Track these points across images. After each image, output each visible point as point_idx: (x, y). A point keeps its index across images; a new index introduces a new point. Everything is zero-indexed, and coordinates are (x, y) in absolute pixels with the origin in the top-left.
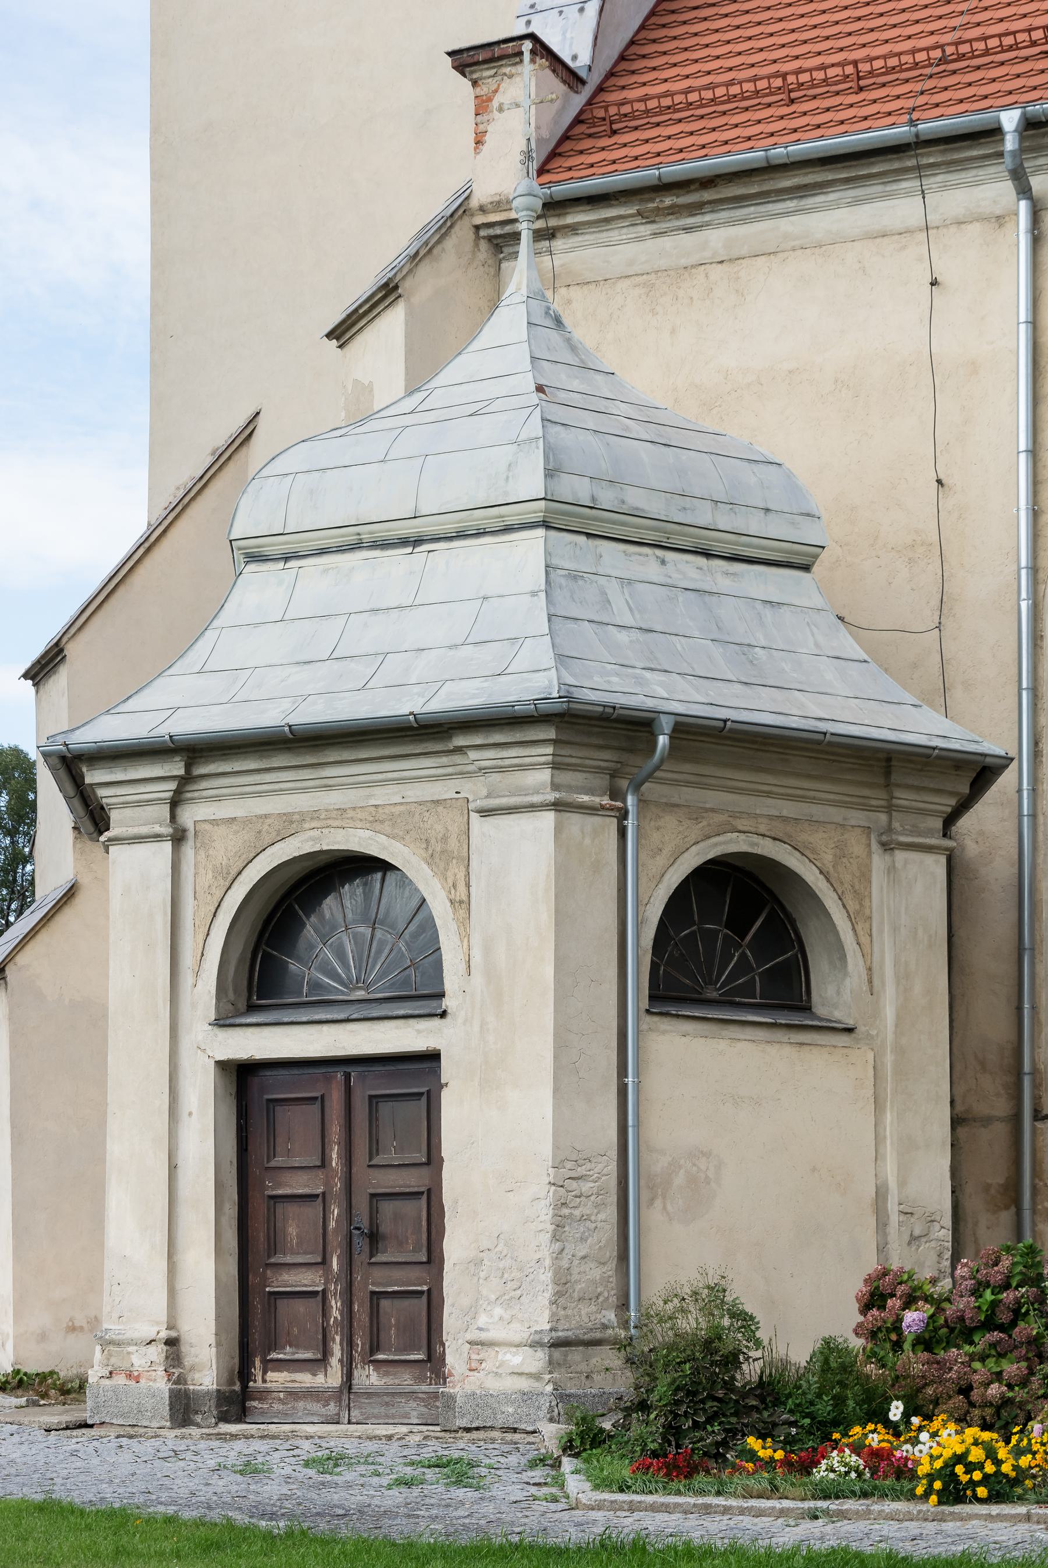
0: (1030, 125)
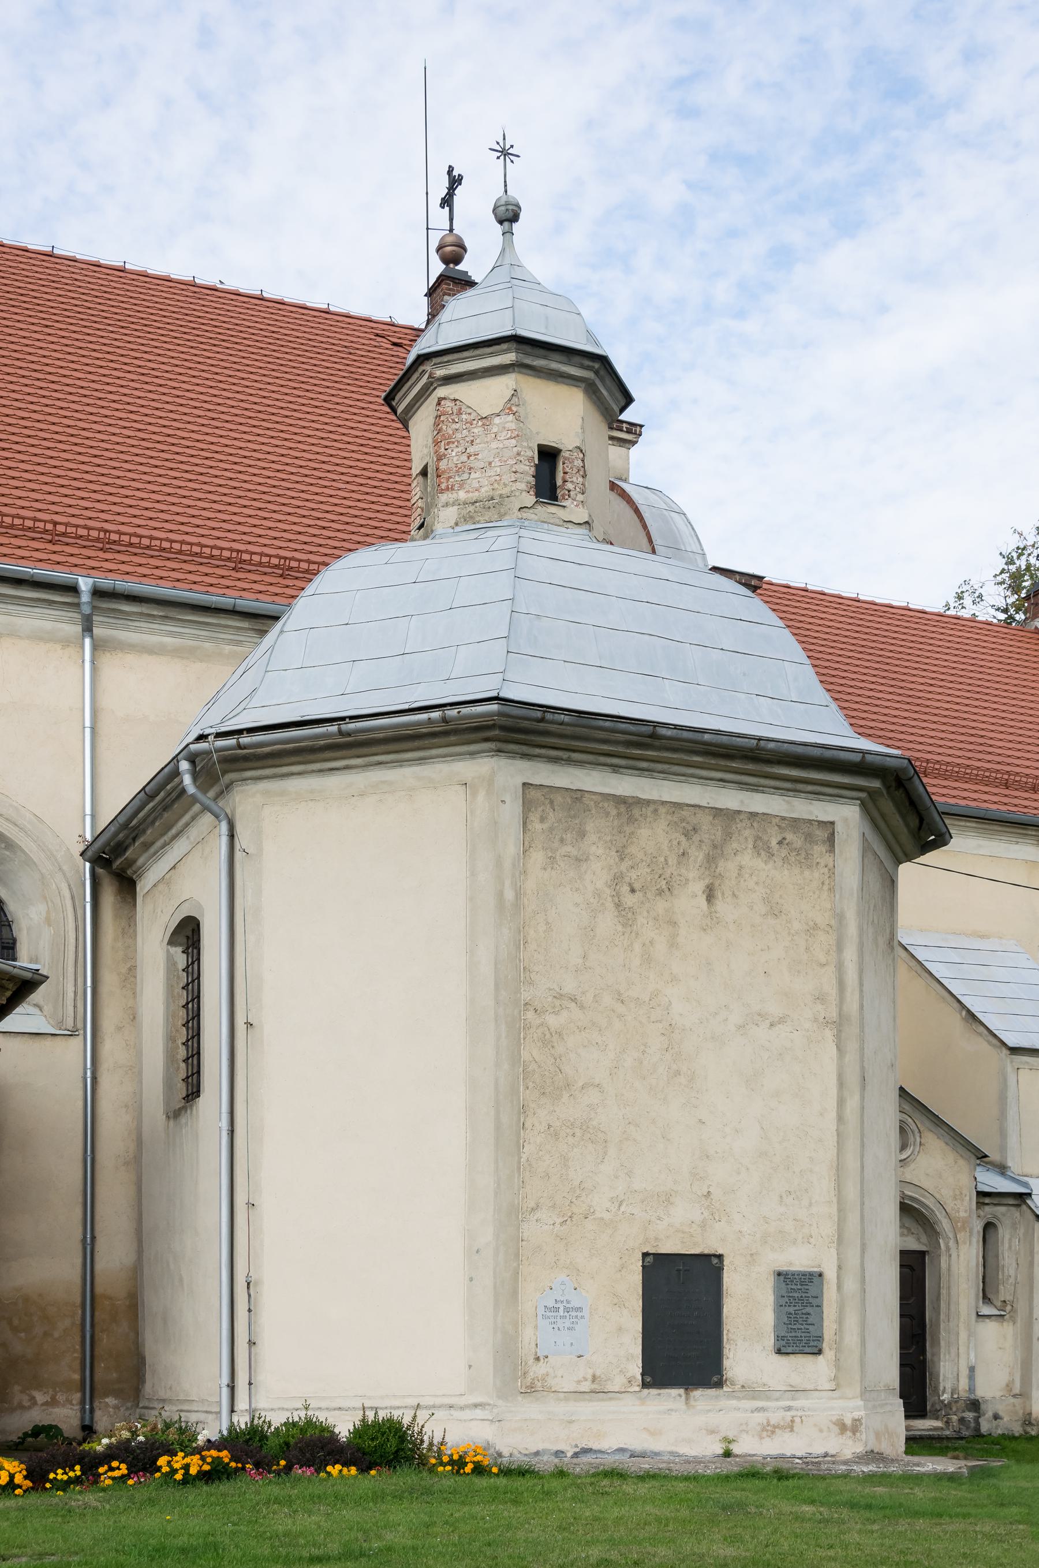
0: (98, 593)
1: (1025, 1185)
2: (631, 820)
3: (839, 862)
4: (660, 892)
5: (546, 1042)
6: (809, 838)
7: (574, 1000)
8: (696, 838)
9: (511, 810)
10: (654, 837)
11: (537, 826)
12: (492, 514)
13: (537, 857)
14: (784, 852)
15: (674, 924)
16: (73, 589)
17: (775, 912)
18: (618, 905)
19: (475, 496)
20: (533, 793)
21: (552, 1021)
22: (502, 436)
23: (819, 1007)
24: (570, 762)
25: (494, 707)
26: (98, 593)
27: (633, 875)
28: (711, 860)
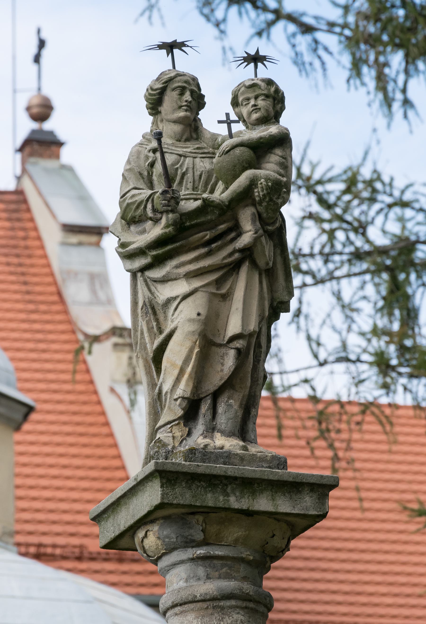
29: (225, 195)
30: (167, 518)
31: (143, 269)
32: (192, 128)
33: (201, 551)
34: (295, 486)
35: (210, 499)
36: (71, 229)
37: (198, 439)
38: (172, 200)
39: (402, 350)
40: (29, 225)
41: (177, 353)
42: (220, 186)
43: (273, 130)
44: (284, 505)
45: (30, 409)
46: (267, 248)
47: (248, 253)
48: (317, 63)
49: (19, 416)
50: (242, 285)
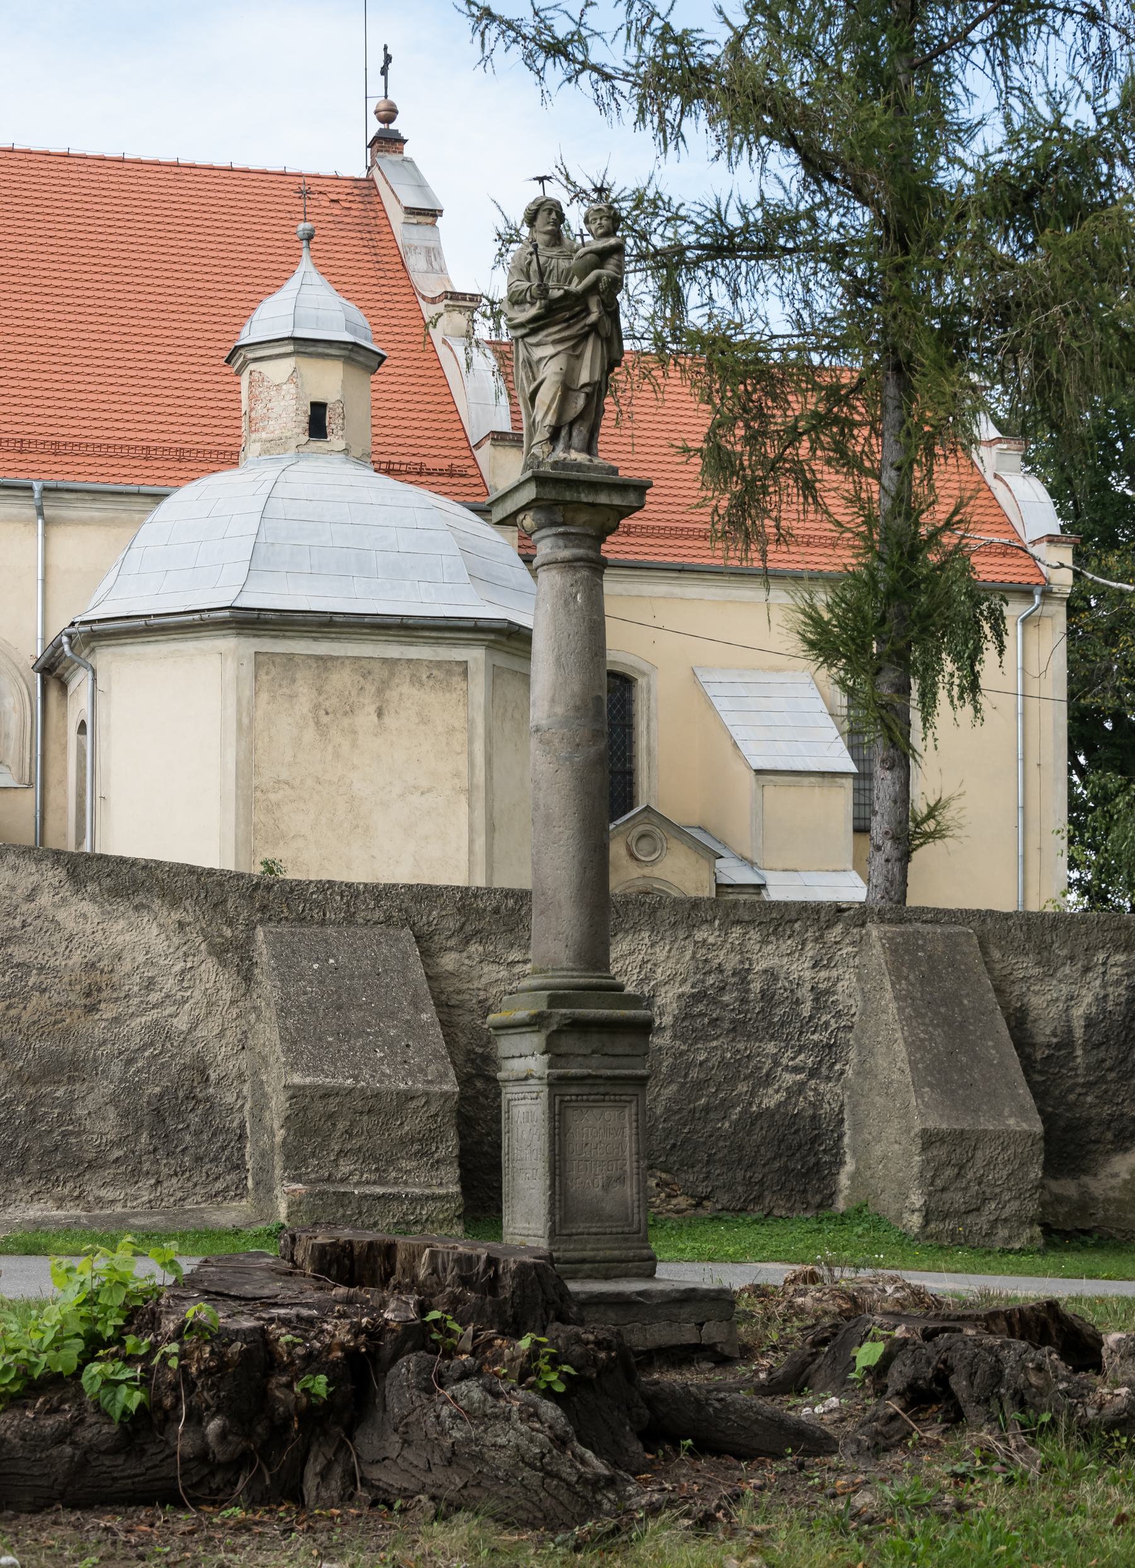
0: (45, 489)
1: (762, 877)
2: (326, 669)
3: (471, 686)
4: (346, 714)
5: (269, 811)
6: (449, 673)
7: (287, 783)
8: (370, 678)
9: (249, 668)
10: (341, 679)
11: (264, 678)
12: (280, 449)
13: (264, 696)
14: (431, 683)
15: (355, 732)
16: (30, 488)
17: (424, 720)
18: (317, 723)
19: (271, 436)
20: (261, 657)
21: (273, 797)
22: (288, 397)
23: (456, 780)
24: (284, 637)
25: (226, 613)
26: (45, 489)
27: (327, 703)
28: (380, 691)
29: (580, 287)
30: (538, 507)
31: (523, 337)
32: (556, 238)
33: (561, 530)
34: (624, 487)
35: (568, 496)
36: (411, 211)
37: (560, 454)
38: (544, 290)
39: (674, 329)
40: (379, 207)
41: (546, 395)
42: (576, 280)
43: (612, 241)
44: (617, 500)
45: (384, 358)
46: (607, 323)
47: (594, 327)
48: (613, 104)
49: (374, 364)
50: (590, 351)
